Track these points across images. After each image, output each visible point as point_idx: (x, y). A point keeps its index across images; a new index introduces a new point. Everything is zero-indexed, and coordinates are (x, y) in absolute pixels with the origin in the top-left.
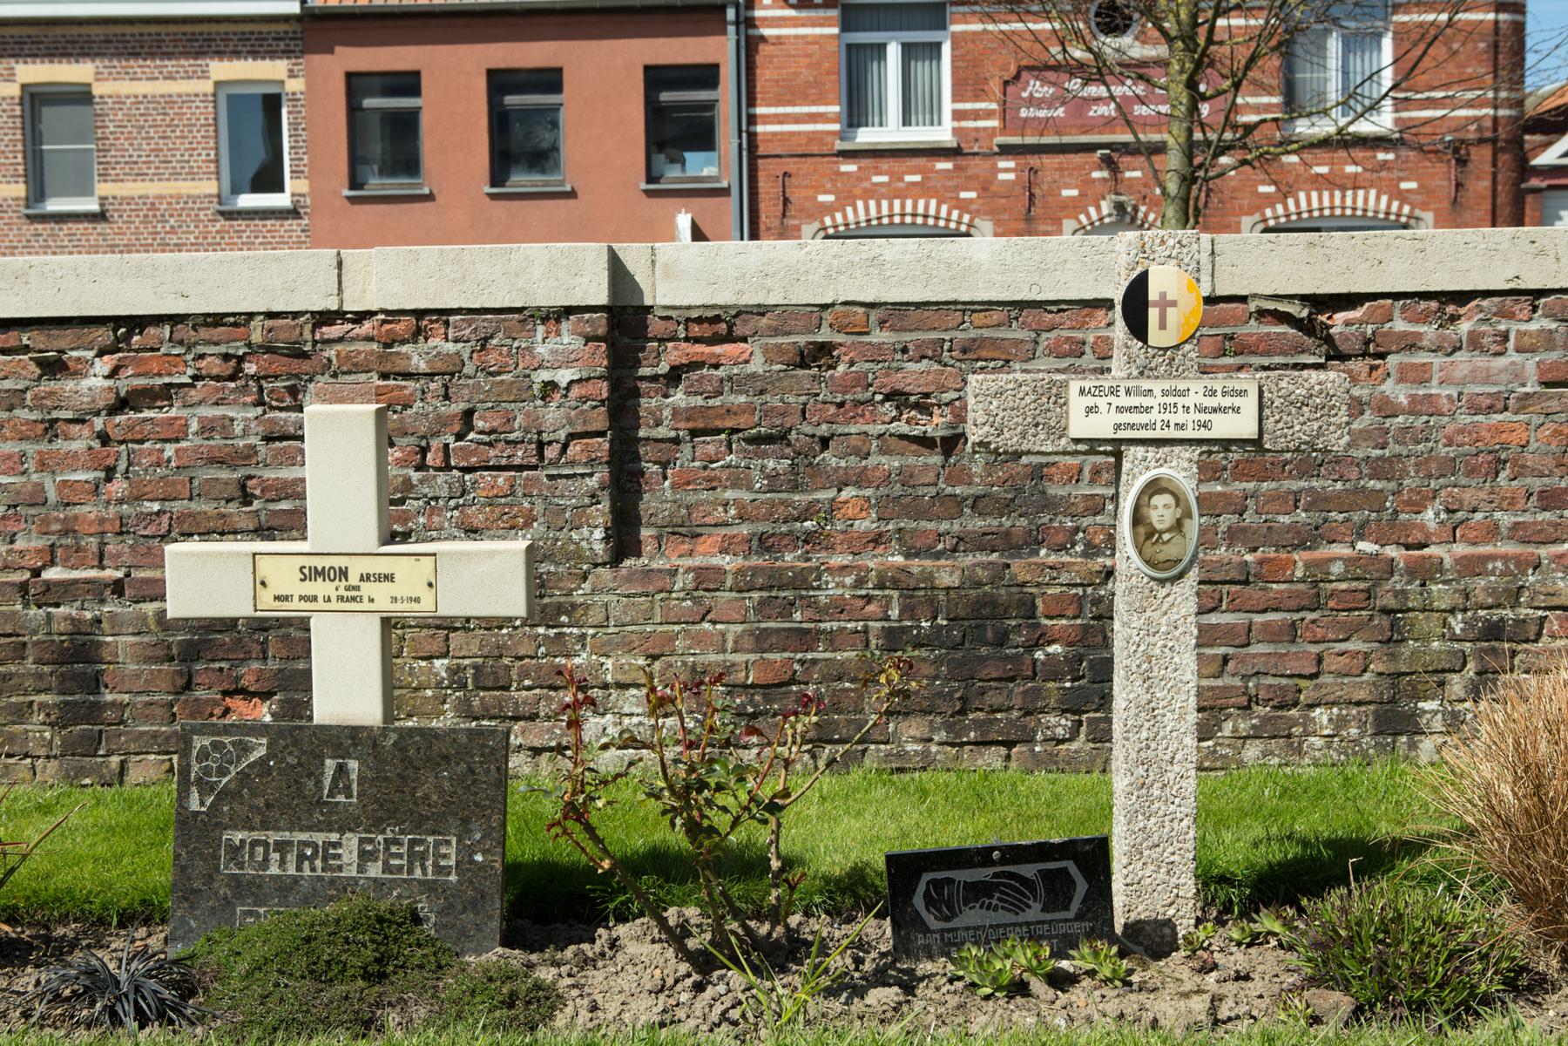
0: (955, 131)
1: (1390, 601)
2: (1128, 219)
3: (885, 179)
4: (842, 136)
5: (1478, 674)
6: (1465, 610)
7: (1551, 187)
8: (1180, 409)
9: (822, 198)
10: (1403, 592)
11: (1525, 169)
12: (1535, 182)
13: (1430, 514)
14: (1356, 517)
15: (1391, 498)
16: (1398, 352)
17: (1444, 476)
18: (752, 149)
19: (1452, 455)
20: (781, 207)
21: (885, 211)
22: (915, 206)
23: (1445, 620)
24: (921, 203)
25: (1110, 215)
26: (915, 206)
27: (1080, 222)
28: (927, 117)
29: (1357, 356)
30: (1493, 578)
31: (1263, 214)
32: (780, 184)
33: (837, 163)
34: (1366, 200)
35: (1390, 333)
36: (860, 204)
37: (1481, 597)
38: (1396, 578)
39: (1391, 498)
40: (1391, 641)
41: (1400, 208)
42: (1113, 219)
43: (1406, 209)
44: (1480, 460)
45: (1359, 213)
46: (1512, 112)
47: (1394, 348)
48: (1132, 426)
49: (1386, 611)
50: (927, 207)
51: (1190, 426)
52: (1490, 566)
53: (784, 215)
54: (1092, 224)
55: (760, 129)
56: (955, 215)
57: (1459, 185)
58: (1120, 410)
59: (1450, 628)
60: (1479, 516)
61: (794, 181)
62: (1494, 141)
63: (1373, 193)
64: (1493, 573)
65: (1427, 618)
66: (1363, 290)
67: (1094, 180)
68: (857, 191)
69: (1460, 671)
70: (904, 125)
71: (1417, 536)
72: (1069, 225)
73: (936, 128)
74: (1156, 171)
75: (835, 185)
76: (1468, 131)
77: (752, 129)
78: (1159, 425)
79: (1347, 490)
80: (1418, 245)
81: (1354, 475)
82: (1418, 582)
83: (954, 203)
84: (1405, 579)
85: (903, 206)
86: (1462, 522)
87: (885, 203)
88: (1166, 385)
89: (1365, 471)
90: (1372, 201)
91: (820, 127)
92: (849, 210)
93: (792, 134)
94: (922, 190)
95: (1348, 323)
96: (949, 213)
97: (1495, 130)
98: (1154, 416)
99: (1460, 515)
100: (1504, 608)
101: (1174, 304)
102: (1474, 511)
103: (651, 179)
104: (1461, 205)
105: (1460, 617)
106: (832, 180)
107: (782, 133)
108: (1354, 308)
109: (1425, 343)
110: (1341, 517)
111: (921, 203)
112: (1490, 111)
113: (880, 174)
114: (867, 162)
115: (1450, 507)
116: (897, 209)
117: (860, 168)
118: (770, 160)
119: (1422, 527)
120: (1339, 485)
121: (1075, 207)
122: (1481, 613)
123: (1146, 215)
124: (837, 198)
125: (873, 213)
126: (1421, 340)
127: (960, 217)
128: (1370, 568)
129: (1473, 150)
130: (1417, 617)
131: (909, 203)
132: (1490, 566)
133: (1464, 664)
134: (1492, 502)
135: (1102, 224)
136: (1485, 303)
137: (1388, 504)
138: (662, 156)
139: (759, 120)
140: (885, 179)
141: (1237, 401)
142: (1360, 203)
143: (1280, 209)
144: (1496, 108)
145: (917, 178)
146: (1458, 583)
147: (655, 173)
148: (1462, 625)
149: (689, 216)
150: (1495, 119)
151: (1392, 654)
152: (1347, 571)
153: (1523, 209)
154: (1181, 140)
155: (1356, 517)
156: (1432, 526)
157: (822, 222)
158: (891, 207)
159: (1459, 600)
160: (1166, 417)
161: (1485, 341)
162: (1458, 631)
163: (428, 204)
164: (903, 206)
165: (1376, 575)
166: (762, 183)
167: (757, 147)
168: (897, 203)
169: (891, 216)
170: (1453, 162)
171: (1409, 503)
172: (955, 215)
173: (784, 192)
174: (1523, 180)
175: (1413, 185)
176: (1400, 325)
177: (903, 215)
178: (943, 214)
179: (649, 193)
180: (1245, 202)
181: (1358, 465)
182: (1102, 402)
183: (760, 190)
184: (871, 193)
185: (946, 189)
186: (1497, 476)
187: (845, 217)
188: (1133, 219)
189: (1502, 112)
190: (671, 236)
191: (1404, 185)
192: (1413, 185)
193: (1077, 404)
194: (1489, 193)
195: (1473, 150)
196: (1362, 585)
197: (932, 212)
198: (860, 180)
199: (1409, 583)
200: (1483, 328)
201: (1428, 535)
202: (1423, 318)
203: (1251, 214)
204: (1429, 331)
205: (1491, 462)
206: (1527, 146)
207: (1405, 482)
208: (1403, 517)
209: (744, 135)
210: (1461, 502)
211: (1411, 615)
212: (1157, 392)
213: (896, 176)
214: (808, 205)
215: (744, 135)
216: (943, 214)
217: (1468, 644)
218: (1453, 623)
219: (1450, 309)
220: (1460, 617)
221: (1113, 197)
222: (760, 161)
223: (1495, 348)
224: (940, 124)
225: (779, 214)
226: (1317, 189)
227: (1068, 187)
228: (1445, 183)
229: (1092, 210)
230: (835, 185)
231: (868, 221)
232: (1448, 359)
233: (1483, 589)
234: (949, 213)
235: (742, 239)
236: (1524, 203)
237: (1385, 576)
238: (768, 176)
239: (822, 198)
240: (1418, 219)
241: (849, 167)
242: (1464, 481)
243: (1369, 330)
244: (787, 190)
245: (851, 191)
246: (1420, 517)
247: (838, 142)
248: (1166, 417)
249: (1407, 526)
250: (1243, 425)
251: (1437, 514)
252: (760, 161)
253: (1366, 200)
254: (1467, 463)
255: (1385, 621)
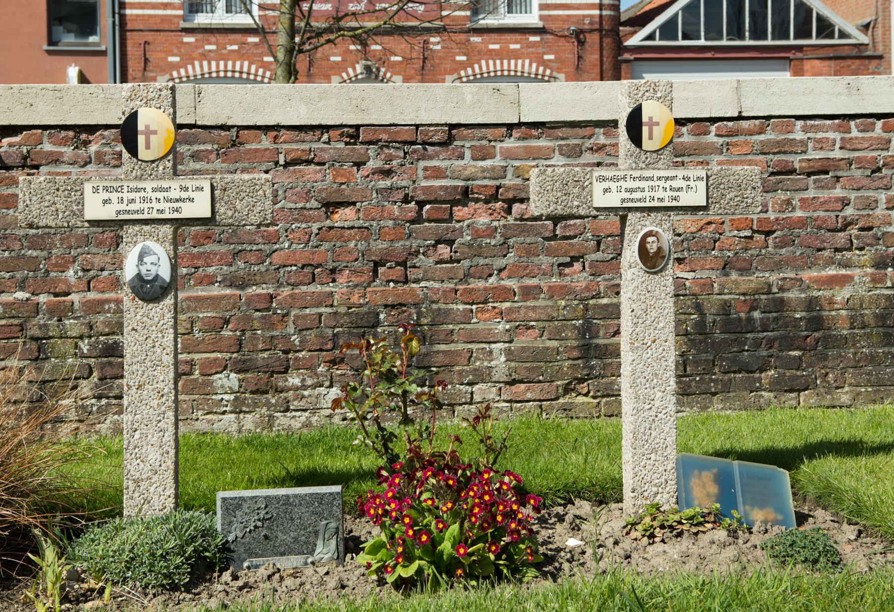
0: (542, 18)
1: (37, 332)
2: (373, 76)
3: (213, 47)
4: (184, 18)
5: (100, 379)
6: (90, 337)
7: (636, 59)
8: (154, 200)
9: (171, 59)
10: (45, 325)
11: (620, 48)
12: (627, 56)
13: (71, 272)
14: (19, 275)
15: (43, 262)
16: (47, 165)
17: (81, 247)
18: (122, 25)
19: (86, 233)
20: (143, 64)
21: (214, 68)
22: (234, 66)
23: (76, 344)
24: (238, 64)
25: (362, 73)
26: (234, 66)
27: (342, 78)
28: (518, 7)
29: (18, 167)
30: (109, 315)
31: (459, 74)
32: (142, 48)
33: (181, 36)
34: (523, 66)
35: (41, 152)
36: (197, 63)
37: (100, 328)
38: (41, 316)
39: (43, 262)
40: (39, 357)
41: (544, 71)
42: (364, 76)
43: (548, 72)
44: (105, 236)
45: (519, 74)
46: (612, 13)
47: (44, 162)
48: (632, 200)
49: (34, 339)
50: (242, 67)
51: (667, 199)
52: (107, 307)
53: (145, 70)
54: (475, 75)
55: (128, 12)
56: (261, 71)
57: (579, 57)
58: (627, 190)
59: (80, 349)
60: (105, 273)
61: (152, 47)
62: (600, 30)
63: (527, 62)
64: (108, 311)
65: (63, 343)
66: (19, 123)
67: (351, 51)
68: (195, 55)
69: (88, 378)
70: (227, 12)
71: (62, 287)
72: (449, 78)
73: (528, 15)
74: (270, 46)
75: (180, 51)
76: (584, 24)
77: (122, 12)
78: (648, 199)
79: (12, 257)
80: (58, 94)
81: (17, 246)
82: (56, 319)
83: (260, 64)
84: (46, 317)
85: (226, 66)
86: (93, 278)
87: (213, 63)
88: (155, 184)
89: (25, 244)
90: (527, 66)
91: (169, 12)
92: (190, 67)
93: (150, 16)
94: (240, 55)
95: (10, 145)
96: (257, 71)
97: (601, 23)
98: (647, 194)
99: (92, 272)
100: (118, 335)
101: (657, 124)
102: (102, 270)
103: (51, 43)
104: (581, 70)
105: (86, 341)
106: (178, 48)
107: (144, 16)
108: (16, 135)
109: (65, 159)
110: (7, 275)
111: (238, 64)
112: (597, 12)
113: (210, 44)
114: (200, 36)
115: (85, 268)
116: (222, 67)
117: (197, 40)
118: (135, 33)
119: (66, 281)
120: (6, 254)
121: (339, 68)
122: (102, 338)
123: (385, 74)
124: (181, 59)
125: (206, 69)
126: (63, 157)
127: (264, 73)
128: (22, 309)
129: (588, 35)
130: (56, 342)
131: (230, 64)
132: (107, 307)
133: (91, 373)
134: (114, 264)
135: (357, 79)
136: (106, 133)
137: (41, 266)
138: (61, 28)
139: (127, 6)
140: (213, 47)
141: (195, 195)
142: (519, 68)
143: (469, 71)
144: (601, 9)
145: (235, 47)
146: (85, 318)
147: (54, 39)
148: (88, 347)
149: (77, 69)
150: (601, 16)
151: (39, 368)
152: (5, 312)
153: (620, 72)
154: (286, 26)
155: (19, 275)
156: (73, 280)
157: (171, 75)
158: (218, 66)
159: (85, 330)
160: (652, 194)
161: (107, 158)
162: (85, 351)
163: (102, 58)
164: (226, 66)
165: (26, 314)
166: (130, 48)
167: (126, 24)
168: (222, 63)
169: (218, 72)
170: (576, 43)
171: (56, 265)
172: (261, 71)
173: (145, 54)
174: (620, 55)
175: (552, 57)
176: (47, 147)
177: (226, 71)
178: (253, 71)
179: (49, 52)
180: (448, 66)
181: (20, 240)
182: (613, 185)
183: (129, 53)
184: (205, 56)
185: (254, 55)
186: (118, 247)
187: (187, 71)
188: (377, 76)
189: (605, 13)
190: (63, 79)
191: (546, 57)
192: (552, 57)
193: (598, 187)
194: (598, 63)
195: (588, 35)
196: (16, 322)
197: (245, 69)
198: (197, 47)
199: (49, 319)
200: (106, 149)
201: (70, 286)
202: (64, 142)
203: (451, 74)
204: (68, 151)
205: (111, 238)
206: (621, 34)
207: (53, 252)
208: (53, 274)
209: (117, 16)
210: (92, 264)
211: (52, 341)
212: (149, 189)
213: (243, 44)
214: (162, 63)
215: (117, 16)
216: (253, 71)
217: (93, 360)
218: (82, 346)
219: (83, 136)
220: (86, 341)
221: (364, 62)
222: (128, 34)
223: (113, 162)
224: (531, 12)
225: (142, 68)
226: (492, 59)
227: (335, 55)
228: (571, 56)
229: (350, 70)
230: (180, 51)
231: (203, 75)
232: (82, 170)
233: (102, 322)
234: (257, 71)
235: (115, 82)
236: (620, 69)
237: (33, 315)
238: (134, 44)
239: (171, 59)
240: (555, 78)
241: (189, 39)
242: (94, 250)
243: (24, 150)
244: (147, 53)
245: (190, 55)
246: (64, 274)
247: (182, 22)
248: (652, 194)
249: (56, 281)
250: (200, 208)
251: (76, 273)
252: (128, 34)
253: (523, 66)
254: (97, 238)
255: (34, 346)
